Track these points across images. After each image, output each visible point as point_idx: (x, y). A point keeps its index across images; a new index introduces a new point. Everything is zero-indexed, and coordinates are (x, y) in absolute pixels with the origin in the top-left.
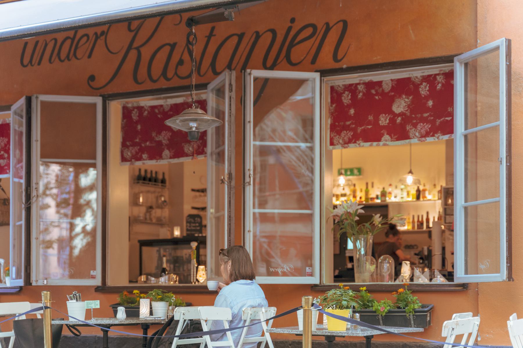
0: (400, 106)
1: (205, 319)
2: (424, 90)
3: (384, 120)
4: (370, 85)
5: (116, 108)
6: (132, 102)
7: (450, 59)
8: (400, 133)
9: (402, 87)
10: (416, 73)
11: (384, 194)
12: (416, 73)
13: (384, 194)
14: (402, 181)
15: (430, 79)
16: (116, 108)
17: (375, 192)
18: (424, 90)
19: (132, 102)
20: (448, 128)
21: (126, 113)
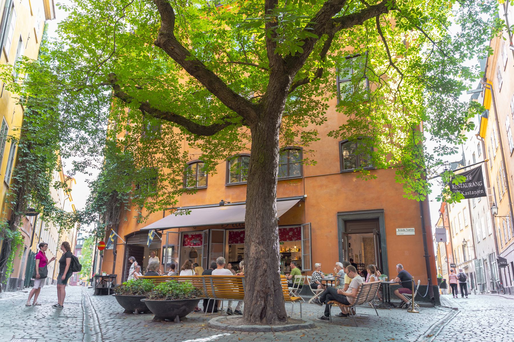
0: (291, 234)
1: (219, 202)
2: (295, 230)
3: (287, 237)
4: (284, 229)
5: (228, 231)
6: (231, 230)
7: (300, 225)
8: (291, 239)
9: (291, 230)
10: (294, 227)
11: (290, 250)
12: (294, 227)
13: (290, 250)
14: (293, 248)
15: (297, 228)
16: (228, 231)
17: (287, 249)
18: (295, 230)
19: (231, 230)
20: (300, 239)
21: (230, 233)
